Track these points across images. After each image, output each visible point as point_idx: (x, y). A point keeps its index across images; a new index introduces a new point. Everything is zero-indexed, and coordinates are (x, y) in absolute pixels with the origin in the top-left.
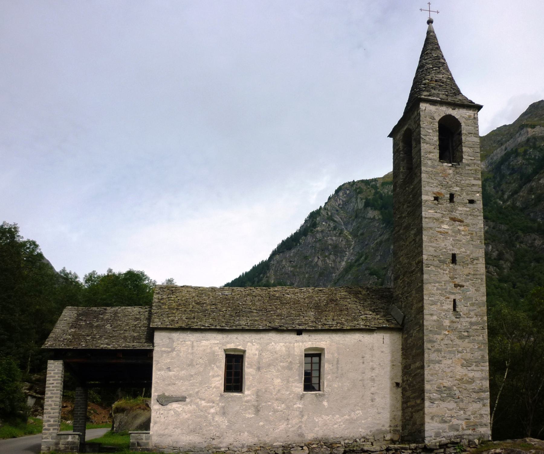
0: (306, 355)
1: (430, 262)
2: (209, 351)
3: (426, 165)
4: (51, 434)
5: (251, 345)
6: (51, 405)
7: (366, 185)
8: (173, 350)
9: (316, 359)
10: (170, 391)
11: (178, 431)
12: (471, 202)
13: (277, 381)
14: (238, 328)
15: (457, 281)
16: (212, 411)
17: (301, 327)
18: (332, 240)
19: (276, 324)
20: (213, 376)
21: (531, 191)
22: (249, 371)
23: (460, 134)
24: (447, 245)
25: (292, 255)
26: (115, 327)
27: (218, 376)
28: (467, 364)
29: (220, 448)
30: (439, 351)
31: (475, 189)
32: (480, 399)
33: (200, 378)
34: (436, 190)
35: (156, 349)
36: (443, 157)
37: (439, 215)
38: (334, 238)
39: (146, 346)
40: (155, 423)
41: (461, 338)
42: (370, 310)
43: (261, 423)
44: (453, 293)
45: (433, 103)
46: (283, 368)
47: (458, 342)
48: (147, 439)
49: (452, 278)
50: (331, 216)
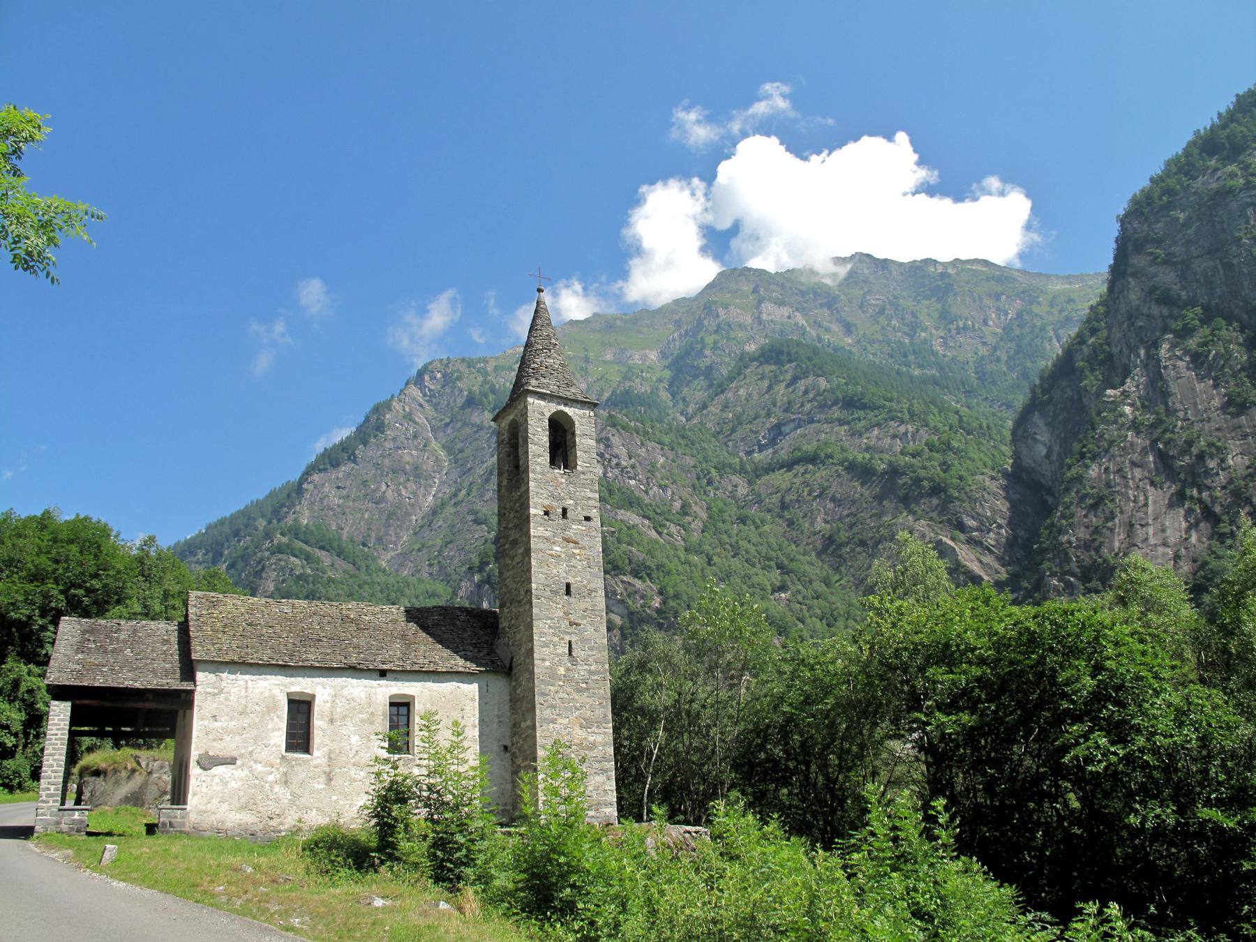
0: (391, 704)
1: (540, 593)
2: (267, 694)
3: (534, 471)
4: (49, 808)
5: (324, 692)
6: (52, 766)
7: (469, 367)
8: (221, 692)
9: (403, 710)
10: (216, 749)
11: (225, 807)
12: (588, 519)
13: (355, 739)
14: (306, 664)
15: (573, 618)
16: (271, 778)
17: (385, 667)
18: (409, 456)
19: (353, 660)
20: (273, 730)
21: (726, 407)
22: (319, 724)
23: (573, 434)
24: (560, 572)
25: (340, 475)
26: (138, 654)
27: (279, 729)
28: (587, 724)
29: (280, 831)
30: (553, 707)
31: (592, 503)
32: (604, 771)
33: (254, 732)
34: (547, 502)
35: (198, 688)
36: (553, 462)
37: (548, 534)
38: (414, 452)
39: (186, 686)
40: (195, 794)
41: (579, 690)
42: (471, 645)
43: (334, 798)
44: (569, 633)
45: (542, 396)
46: (362, 721)
47: (575, 696)
48: (182, 817)
49: (567, 614)
50: (410, 414)
